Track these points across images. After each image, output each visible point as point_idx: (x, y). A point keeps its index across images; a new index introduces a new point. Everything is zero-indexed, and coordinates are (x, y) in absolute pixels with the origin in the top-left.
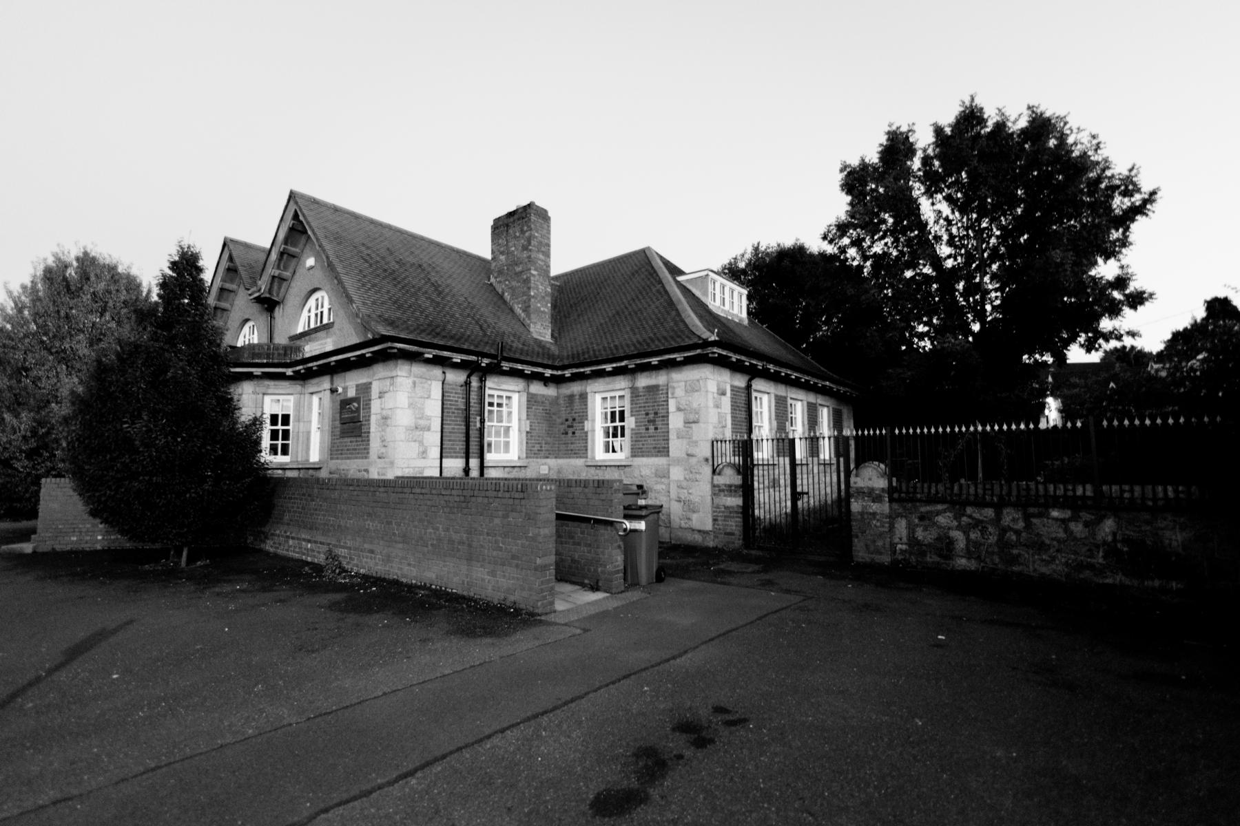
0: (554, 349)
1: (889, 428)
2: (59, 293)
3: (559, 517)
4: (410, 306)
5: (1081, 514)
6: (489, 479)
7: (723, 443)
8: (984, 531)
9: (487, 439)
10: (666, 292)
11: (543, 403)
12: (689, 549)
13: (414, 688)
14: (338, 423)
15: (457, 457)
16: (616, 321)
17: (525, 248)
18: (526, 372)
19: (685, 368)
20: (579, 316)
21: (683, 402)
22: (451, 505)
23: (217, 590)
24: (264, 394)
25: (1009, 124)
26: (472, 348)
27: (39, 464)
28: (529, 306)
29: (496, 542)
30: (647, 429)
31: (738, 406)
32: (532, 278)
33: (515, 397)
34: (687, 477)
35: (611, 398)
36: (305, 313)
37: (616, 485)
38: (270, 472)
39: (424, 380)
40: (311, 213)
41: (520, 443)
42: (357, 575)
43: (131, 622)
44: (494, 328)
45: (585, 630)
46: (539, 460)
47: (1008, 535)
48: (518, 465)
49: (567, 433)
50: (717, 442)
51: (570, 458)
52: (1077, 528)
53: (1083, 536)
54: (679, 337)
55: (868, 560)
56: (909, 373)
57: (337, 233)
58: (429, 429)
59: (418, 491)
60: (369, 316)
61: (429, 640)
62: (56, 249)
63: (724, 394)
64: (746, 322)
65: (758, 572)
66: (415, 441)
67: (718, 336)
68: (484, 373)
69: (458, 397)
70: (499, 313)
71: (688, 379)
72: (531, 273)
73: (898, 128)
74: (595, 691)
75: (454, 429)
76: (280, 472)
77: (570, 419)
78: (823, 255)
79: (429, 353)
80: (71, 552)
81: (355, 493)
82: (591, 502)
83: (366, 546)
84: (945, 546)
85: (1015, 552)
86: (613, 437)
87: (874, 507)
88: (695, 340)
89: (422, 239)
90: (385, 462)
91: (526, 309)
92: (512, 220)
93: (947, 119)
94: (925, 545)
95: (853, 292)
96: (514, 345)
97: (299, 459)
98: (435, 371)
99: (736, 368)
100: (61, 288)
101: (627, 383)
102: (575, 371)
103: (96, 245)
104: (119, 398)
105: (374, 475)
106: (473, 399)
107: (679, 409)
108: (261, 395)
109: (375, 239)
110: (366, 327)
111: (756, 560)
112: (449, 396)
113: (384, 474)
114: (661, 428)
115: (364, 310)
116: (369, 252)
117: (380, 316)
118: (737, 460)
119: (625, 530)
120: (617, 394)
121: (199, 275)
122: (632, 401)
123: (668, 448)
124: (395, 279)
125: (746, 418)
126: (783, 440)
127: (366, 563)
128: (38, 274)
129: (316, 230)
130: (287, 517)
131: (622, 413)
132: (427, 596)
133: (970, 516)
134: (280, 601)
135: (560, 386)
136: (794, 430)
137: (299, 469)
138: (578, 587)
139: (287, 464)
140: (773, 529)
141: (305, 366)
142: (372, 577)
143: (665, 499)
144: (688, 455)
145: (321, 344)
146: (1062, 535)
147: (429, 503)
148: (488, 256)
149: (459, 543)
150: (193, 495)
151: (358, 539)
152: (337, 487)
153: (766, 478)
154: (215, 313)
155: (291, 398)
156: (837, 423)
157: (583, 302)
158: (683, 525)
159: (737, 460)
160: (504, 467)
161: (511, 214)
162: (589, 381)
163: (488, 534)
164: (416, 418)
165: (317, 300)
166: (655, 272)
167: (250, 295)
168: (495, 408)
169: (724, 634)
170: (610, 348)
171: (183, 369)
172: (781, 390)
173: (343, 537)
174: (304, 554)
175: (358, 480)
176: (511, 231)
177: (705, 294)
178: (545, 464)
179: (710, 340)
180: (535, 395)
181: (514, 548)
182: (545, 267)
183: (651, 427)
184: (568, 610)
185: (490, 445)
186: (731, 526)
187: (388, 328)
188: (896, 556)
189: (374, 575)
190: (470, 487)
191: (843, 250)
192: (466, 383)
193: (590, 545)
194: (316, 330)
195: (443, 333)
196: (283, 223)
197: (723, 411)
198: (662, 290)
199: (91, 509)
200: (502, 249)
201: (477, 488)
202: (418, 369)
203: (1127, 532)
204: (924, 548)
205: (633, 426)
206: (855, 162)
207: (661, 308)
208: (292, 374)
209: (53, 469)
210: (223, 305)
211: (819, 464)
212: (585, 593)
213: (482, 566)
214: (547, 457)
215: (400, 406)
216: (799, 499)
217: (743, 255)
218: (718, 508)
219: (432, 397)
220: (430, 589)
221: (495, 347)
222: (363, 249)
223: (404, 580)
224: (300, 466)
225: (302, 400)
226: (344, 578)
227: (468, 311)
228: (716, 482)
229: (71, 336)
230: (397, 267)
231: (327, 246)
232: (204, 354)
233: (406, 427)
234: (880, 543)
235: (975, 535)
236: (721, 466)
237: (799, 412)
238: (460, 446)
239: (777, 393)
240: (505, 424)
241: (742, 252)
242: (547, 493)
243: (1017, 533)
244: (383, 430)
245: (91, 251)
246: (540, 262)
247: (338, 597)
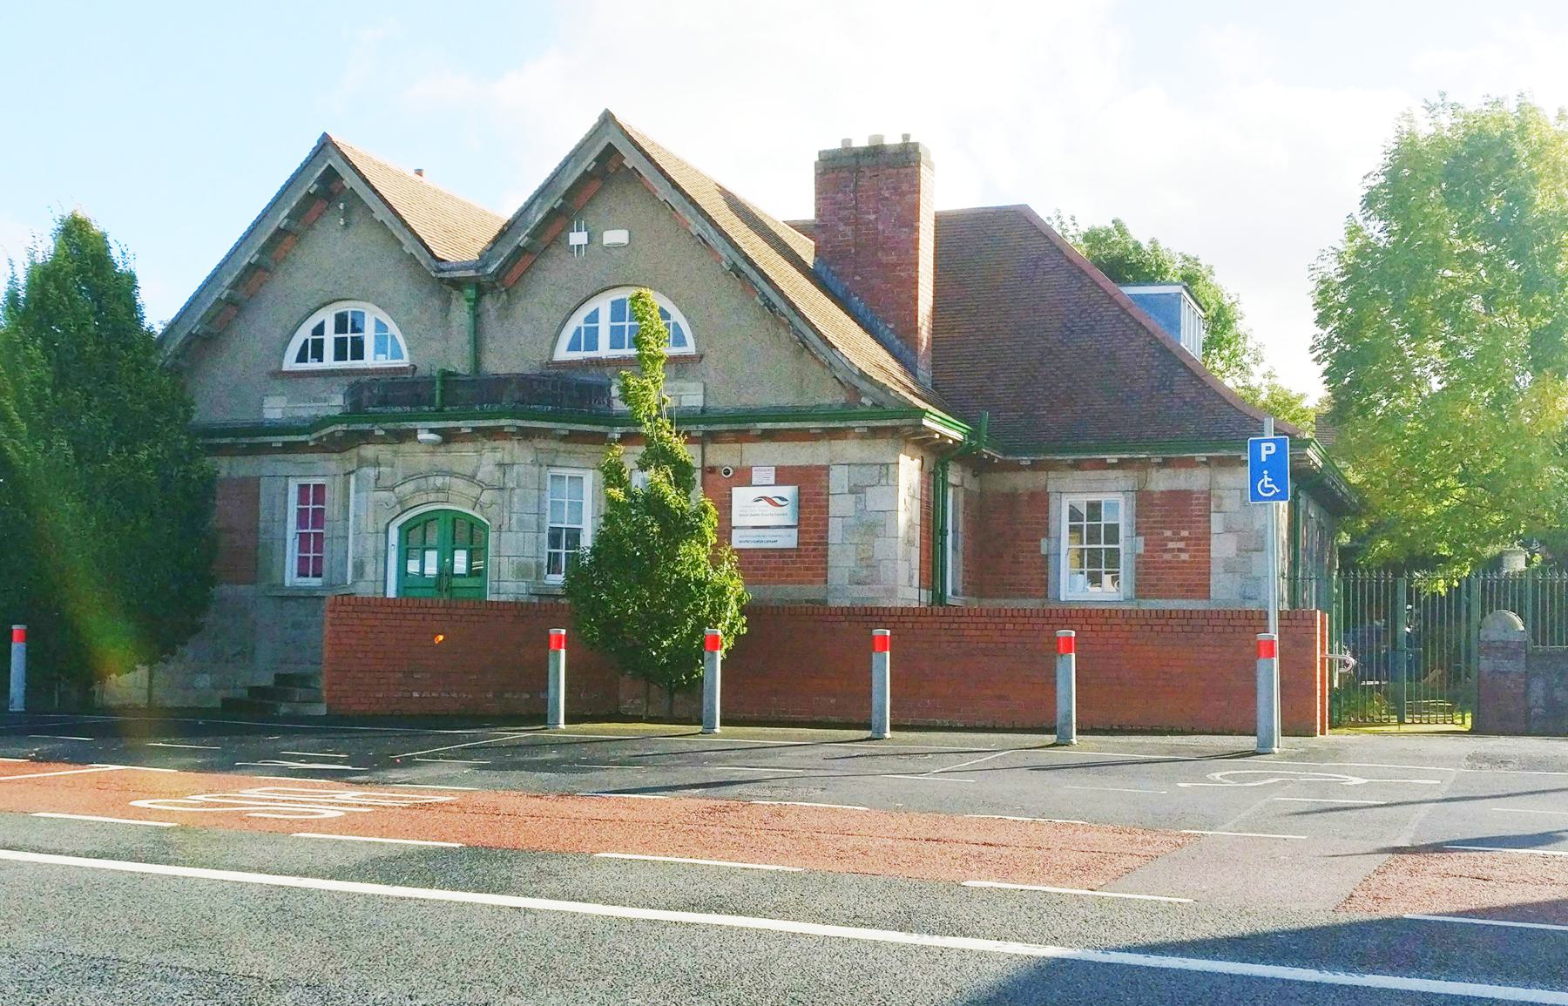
107: (1228, 530)
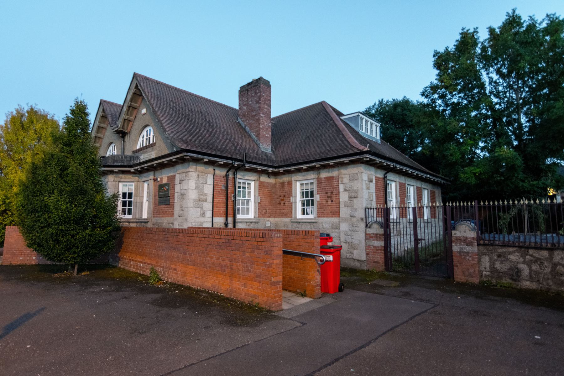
0: (273, 157)
1: (476, 201)
2: (18, 130)
3: (284, 252)
4: (196, 134)
6: (239, 229)
7: (370, 209)
8: (541, 264)
9: (237, 207)
10: (336, 125)
11: (267, 186)
12: (353, 271)
13: (203, 362)
14: (157, 197)
15: (221, 217)
16: (308, 141)
17: (257, 102)
18: (258, 169)
19: (350, 166)
20: (286, 139)
21: (348, 186)
22: (220, 244)
23: (91, 290)
24: (119, 182)
25: (537, 25)
26: (229, 156)
27: (6, 218)
28: (260, 134)
29: (247, 267)
30: (327, 201)
31: (379, 189)
32: (261, 118)
33: (252, 184)
34: (350, 229)
35: (305, 184)
36: (141, 139)
37: (316, 234)
38: (121, 223)
39: (204, 174)
40: (144, 85)
41: (255, 209)
42: (167, 282)
43: (43, 309)
44: (241, 145)
45: (304, 324)
46: (265, 218)
47: (558, 268)
48: (254, 221)
49: (280, 204)
50: (368, 209)
51: (282, 217)
54: (345, 149)
56: (478, 170)
57: (158, 95)
58: (206, 201)
59: (202, 236)
60: (175, 139)
61: (210, 327)
62: (17, 107)
63: (371, 181)
64: (379, 142)
65: (398, 286)
67: (369, 148)
68: (237, 169)
69: (222, 183)
70: (243, 138)
71: (351, 173)
72: (260, 116)
73: (468, 31)
74: (319, 370)
75: (219, 201)
76: (127, 224)
77: (282, 196)
78: (423, 105)
80: (19, 266)
81: (167, 236)
82: (301, 244)
83: (173, 266)
84: (516, 274)
86: (307, 206)
87: (468, 249)
88: (356, 151)
89: (202, 98)
90: (182, 219)
91: (258, 135)
92: (250, 87)
93: (497, 23)
94: (502, 273)
95: (441, 124)
96: (252, 155)
97: (137, 217)
98: (209, 169)
99: (379, 167)
100: (19, 127)
101: (315, 176)
102: (285, 169)
103: (37, 105)
104: (43, 183)
105: (176, 226)
106: (230, 184)
107: (345, 190)
108: (117, 183)
109: (178, 98)
110: (173, 145)
111: (395, 279)
112: (217, 183)
113: (182, 226)
114: (335, 201)
115: (172, 135)
116: (174, 105)
117: (180, 139)
118: (380, 219)
119: (322, 261)
120: (309, 182)
121: (86, 117)
122: (318, 185)
123: (339, 212)
124: (188, 119)
125: (383, 196)
126: (379, 208)
127: (172, 276)
128: (8, 120)
129: (147, 93)
130: (130, 249)
131: (312, 193)
132: (207, 297)
133: (531, 256)
134: (126, 298)
135: (277, 177)
136: (409, 203)
137: (137, 222)
138: (294, 294)
139: (130, 219)
140: (399, 260)
141: (140, 167)
142: (175, 284)
143: (337, 241)
144: (351, 216)
145: (149, 155)
147: (208, 243)
148: (237, 107)
149: (225, 266)
150: (81, 236)
151: (168, 262)
152: (157, 233)
153: (395, 230)
154: (95, 140)
155: (133, 184)
156: (432, 198)
157: (288, 131)
158: (348, 256)
159: (380, 219)
161: (249, 84)
162: (293, 175)
163: (242, 262)
165: (147, 131)
166: (329, 114)
167: (113, 129)
168: (242, 190)
169: (391, 330)
170: (305, 156)
171: (76, 168)
172: (402, 179)
173: (160, 260)
174: (138, 269)
175: (168, 229)
176: (249, 93)
177: (358, 126)
178: (268, 221)
179: (364, 150)
180: (263, 182)
181: (258, 271)
182: (268, 112)
183: (329, 200)
184: (290, 309)
185: (238, 210)
186: (378, 258)
187: (185, 145)
188: (482, 279)
189: (177, 283)
190: (231, 235)
191: (434, 101)
192: (226, 175)
193: (300, 269)
194: (147, 147)
195: (214, 148)
196: (130, 91)
197: (371, 191)
198: (333, 124)
199: (28, 243)
200: (245, 103)
201: (236, 235)
202: (201, 168)
204: (501, 274)
205: (319, 199)
206: (442, 50)
207: (333, 134)
208: (133, 171)
209: (13, 221)
210: (100, 135)
211: (424, 222)
212: (296, 297)
213: (239, 281)
214: (270, 217)
215: (191, 188)
216: (419, 243)
217: (374, 106)
220: (208, 292)
221: (242, 155)
222: (171, 103)
223: (193, 287)
224: (137, 221)
225: (139, 185)
226: (160, 284)
227: (227, 136)
228: (368, 232)
229: (24, 151)
230: (189, 113)
231: (153, 102)
232: (88, 160)
233: (194, 200)
235: (535, 267)
236: (370, 223)
237: (412, 192)
238: (223, 210)
240: (246, 198)
241: (373, 104)
242: (278, 238)
244: (181, 201)
245: (35, 107)
246: (265, 110)
247: (157, 296)
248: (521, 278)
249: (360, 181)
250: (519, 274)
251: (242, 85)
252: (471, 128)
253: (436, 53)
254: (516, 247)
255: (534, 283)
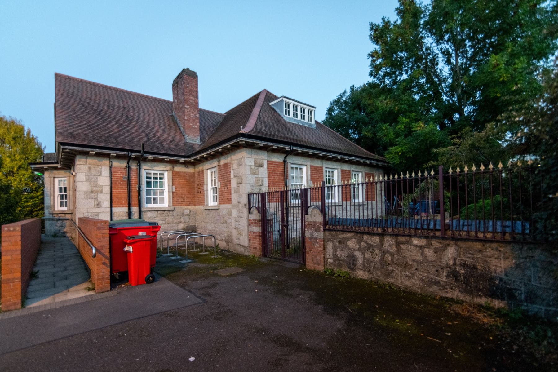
5: (433, 242)
8: (373, 252)
11: (184, 176)
15: (123, 207)
32: (186, 110)
33: (166, 174)
39: (96, 166)
46: (182, 207)
51: (200, 205)
52: (429, 253)
53: (433, 260)
55: (313, 268)
63: (261, 166)
66: (92, 199)
69: (122, 175)
71: (238, 158)
79: (93, 151)
84: (352, 262)
85: (390, 268)
87: (316, 234)
94: (341, 260)
98: (104, 161)
106: (133, 175)
107: (235, 177)
133: (366, 242)
139: (65, 211)
146: (419, 258)
160: (157, 211)
161: (178, 77)
164: (91, 186)
202: (91, 161)
203: (464, 258)
214: (188, 205)
215: (80, 180)
218: (251, 233)
219: (102, 175)
233: (85, 192)
234: (318, 258)
238: (125, 201)
239: (312, 165)
243: (392, 255)
246: (191, 101)
248: (356, 266)
249: (244, 166)
250: (355, 262)
251: (174, 79)
252: (402, 104)
253: (373, 27)
254: (353, 232)
255: (366, 273)
